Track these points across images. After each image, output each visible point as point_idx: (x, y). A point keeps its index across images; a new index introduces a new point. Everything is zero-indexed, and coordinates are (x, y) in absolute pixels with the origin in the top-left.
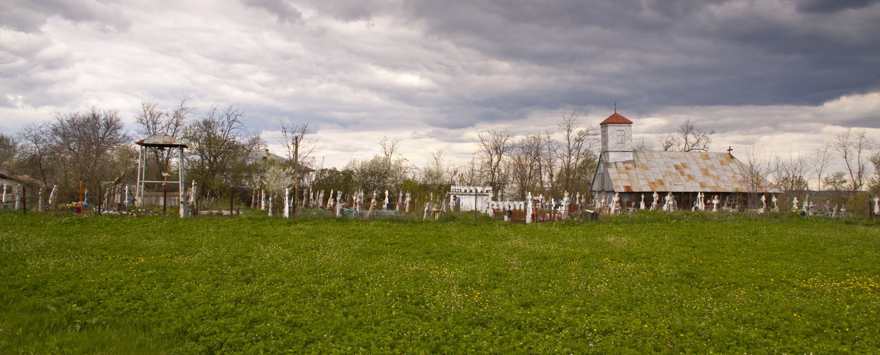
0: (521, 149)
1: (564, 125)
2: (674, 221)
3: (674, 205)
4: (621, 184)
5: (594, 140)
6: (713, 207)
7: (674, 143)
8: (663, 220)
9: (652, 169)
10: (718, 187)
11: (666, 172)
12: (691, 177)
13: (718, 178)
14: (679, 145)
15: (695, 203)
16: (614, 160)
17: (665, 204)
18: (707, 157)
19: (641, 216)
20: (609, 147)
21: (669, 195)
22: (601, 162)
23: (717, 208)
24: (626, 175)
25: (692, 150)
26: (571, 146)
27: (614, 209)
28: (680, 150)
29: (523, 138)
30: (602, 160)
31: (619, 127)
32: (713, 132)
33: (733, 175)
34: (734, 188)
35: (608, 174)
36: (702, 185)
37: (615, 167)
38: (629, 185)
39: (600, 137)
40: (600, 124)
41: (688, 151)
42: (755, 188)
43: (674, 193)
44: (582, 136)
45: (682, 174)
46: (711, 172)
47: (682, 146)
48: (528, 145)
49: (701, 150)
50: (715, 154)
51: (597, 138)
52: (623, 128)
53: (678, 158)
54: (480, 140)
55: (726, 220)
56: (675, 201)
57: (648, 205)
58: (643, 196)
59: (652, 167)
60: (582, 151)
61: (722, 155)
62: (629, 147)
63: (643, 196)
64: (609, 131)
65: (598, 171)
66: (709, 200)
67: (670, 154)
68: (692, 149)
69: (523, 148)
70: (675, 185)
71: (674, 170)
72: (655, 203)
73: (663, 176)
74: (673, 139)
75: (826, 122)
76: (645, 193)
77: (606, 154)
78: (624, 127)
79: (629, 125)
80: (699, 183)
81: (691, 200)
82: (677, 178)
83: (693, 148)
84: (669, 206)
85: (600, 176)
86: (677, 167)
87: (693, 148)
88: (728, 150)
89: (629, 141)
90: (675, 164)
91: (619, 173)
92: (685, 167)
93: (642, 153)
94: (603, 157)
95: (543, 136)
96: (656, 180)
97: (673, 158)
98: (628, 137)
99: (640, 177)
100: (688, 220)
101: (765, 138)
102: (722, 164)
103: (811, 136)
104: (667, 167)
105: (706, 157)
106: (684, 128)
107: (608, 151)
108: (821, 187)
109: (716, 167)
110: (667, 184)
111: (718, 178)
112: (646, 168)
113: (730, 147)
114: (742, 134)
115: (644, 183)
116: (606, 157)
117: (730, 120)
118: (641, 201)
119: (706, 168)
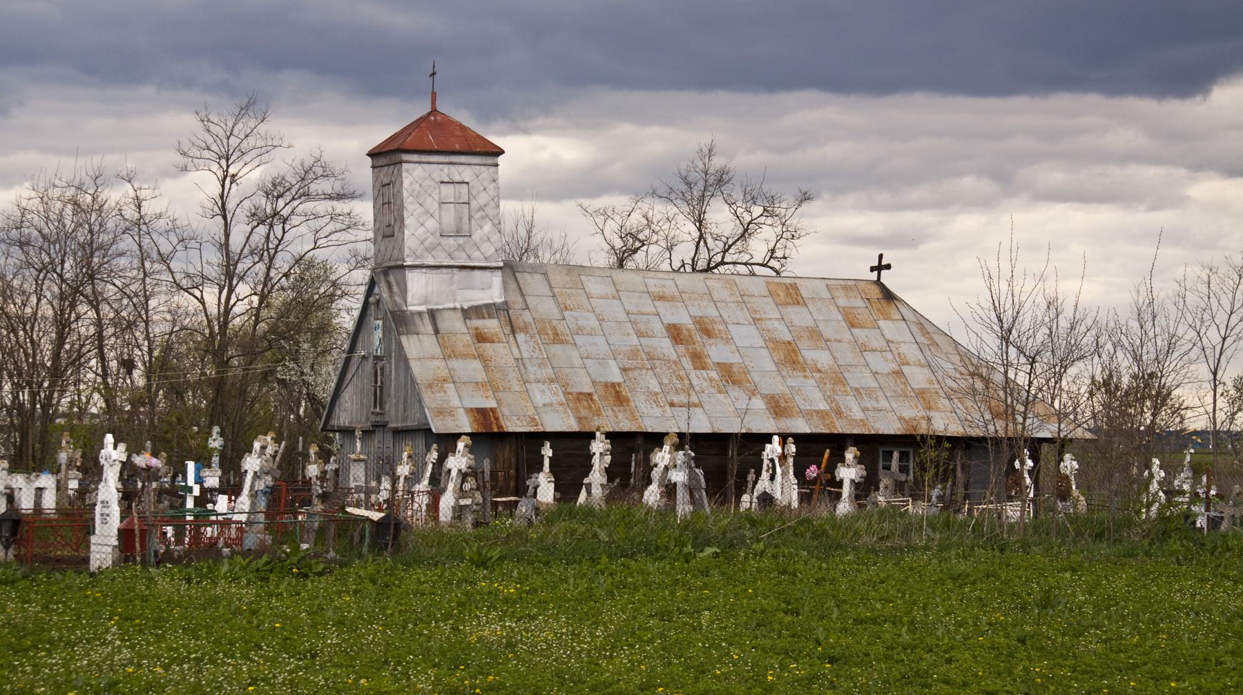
0: (16, 250)
1: (206, 154)
2: (709, 550)
3: (691, 489)
4: (456, 402)
5: (333, 217)
6: (839, 496)
7: (655, 238)
8: (667, 549)
9: (579, 340)
10: (839, 413)
11: (634, 354)
12: (730, 376)
13: (836, 379)
14: (670, 249)
15: (751, 477)
16: (426, 302)
17: (649, 482)
18: (791, 294)
19: (573, 532)
20: (407, 251)
21: (667, 448)
22: (372, 309)
23: (857, 497)
24: (477, 365)
25: (722, 269)
26: (236, 241)
27: (452, 502)
28: (676, 265)
29: (24, 203)
30: (378, 302)
31: (446, 168)
32: (805, 198)
33: (895, 366)
34: (901, 419)
35: (404, 360)
36: (777, 407)
37: (430, 329)
38: (491, 404)
39: (364, 210)
40: (372, 154)
41: (708, 269)
42: (1020, 419)
43: (683, 440)
44: (281, 203)
45: (698, 360)
46: (810, 354)
47: (684, 252)
48: (46, 231)
49: (757, 269)
50: (821, 285)
51: (346, 210)
52: (466, 173)
53: (679, 298)
54: (767, 293)
55: (913, 549)
56: (700, 472)
57: (568, 485)
58: (547, 451)
59: (580, 330)
60: (283, 262)
61: (850, 286)
62: (489, 249)
63: (547, 451)
64: (406, 183)
65: (360, 345)
66: (813, 467)
67: (651, 282)
68: (723, 263)
69: (23, 244)
70: (672, 405)
71: (665, 346)
72: (597, 478)
73: (624, 370)
74: (649, 223)
75: (1200, 166)
76: (555, 437)
77: (392, 279)
78: (467, 170)
79: (490, 160)
80: (764, 397)
81: (733, 468)
82: (680, 378)
83: (728, 259)
84: (670, 490)
85: (369, 365)
86: (675, 334)
87: (728, 259)
88: (872, 269)
89: (488, 227)
90: (670, 319)
91: (446, 357)
92: (708, 333)
93: (538, 278)
94: (382, 290)
95: (116, 195)
96: (593, 382)
97: (661, 298)
98: (481, 208)
99: (533, 371)
100: (761, 545)
101: (966, 223)
102: (852, 325)
103: (1142, 218)
104: (640, 334)
105: (788, 294)
106: (693, 176)
107: (402, 267)
108: (1220, 416)
109: (828, 333)
110: (640, 402)
111: (836, 379)
112: (557, 338)
113: (881, 257)
114: (874, 207)
115: (547, 399)
116: (395, 289)
117: (833, 151)
118: (540, 469)
119: (788, 337)
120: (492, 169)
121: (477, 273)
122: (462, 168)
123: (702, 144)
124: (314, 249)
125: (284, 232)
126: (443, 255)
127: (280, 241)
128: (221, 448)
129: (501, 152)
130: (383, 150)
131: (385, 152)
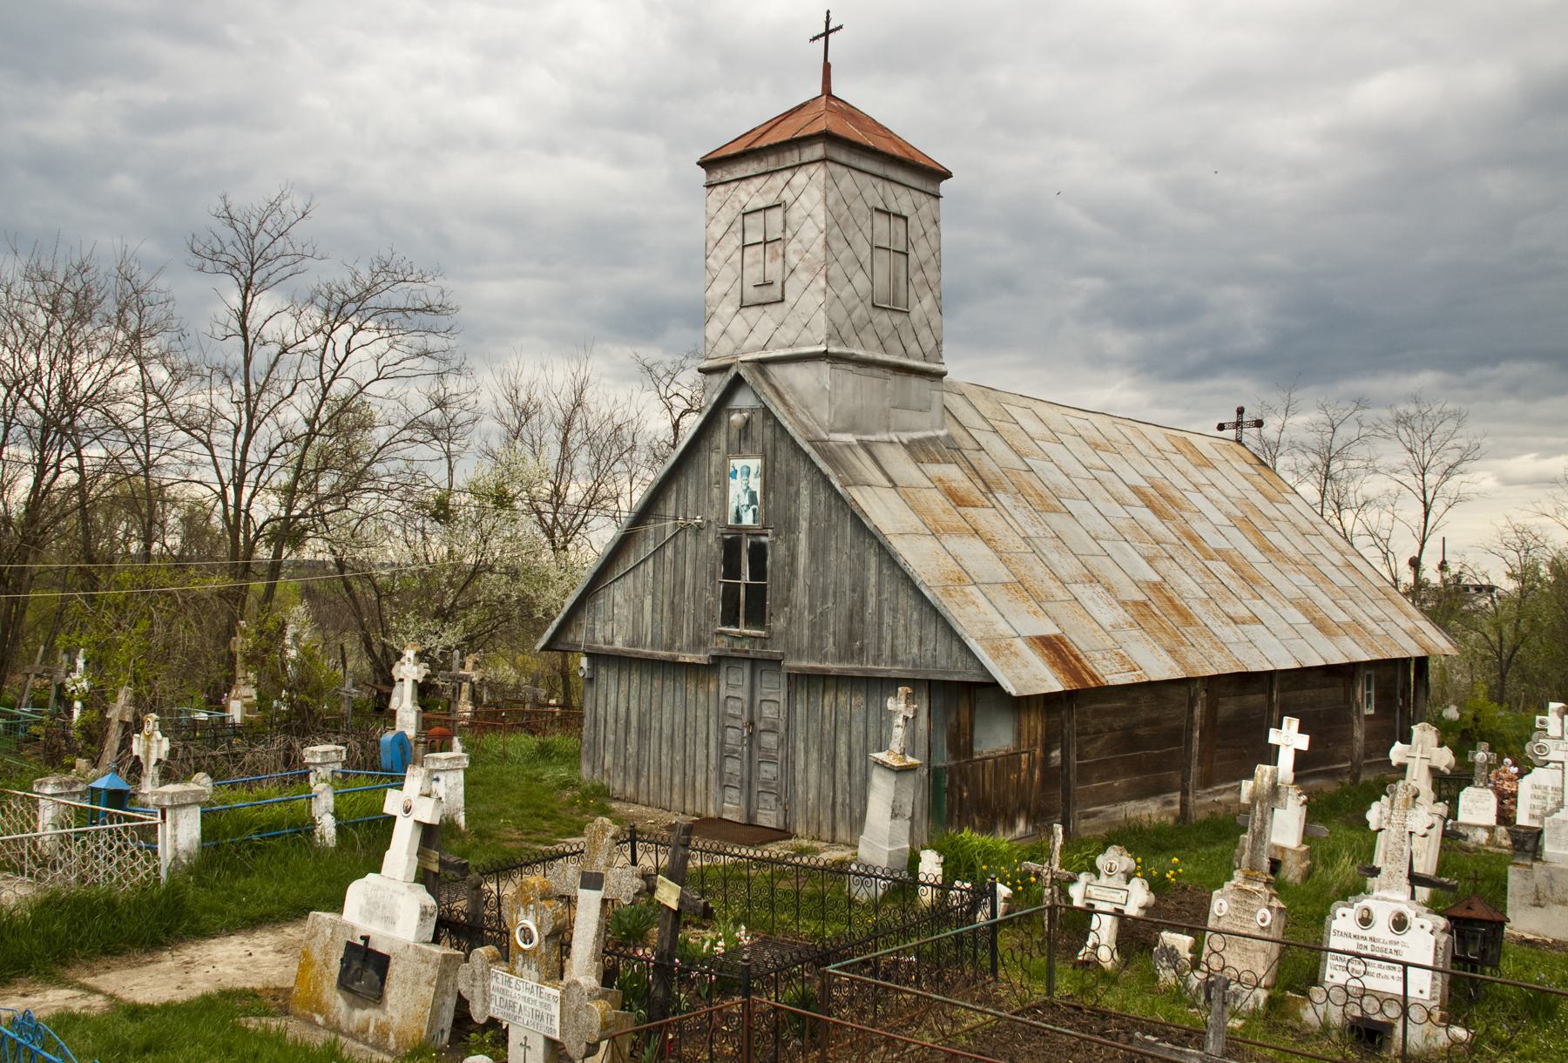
31: (880, 184)
120: (933, 201)
121: (915, 382)
122: (899, 190)
123: (524, 381)
124: (377, 379)
125: (348, 353)
126: (874, 342)
127: (340, 365)
128: (1305, 848)
129: (946, 175)
130: (763, 143)
131: (762, 149)
